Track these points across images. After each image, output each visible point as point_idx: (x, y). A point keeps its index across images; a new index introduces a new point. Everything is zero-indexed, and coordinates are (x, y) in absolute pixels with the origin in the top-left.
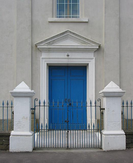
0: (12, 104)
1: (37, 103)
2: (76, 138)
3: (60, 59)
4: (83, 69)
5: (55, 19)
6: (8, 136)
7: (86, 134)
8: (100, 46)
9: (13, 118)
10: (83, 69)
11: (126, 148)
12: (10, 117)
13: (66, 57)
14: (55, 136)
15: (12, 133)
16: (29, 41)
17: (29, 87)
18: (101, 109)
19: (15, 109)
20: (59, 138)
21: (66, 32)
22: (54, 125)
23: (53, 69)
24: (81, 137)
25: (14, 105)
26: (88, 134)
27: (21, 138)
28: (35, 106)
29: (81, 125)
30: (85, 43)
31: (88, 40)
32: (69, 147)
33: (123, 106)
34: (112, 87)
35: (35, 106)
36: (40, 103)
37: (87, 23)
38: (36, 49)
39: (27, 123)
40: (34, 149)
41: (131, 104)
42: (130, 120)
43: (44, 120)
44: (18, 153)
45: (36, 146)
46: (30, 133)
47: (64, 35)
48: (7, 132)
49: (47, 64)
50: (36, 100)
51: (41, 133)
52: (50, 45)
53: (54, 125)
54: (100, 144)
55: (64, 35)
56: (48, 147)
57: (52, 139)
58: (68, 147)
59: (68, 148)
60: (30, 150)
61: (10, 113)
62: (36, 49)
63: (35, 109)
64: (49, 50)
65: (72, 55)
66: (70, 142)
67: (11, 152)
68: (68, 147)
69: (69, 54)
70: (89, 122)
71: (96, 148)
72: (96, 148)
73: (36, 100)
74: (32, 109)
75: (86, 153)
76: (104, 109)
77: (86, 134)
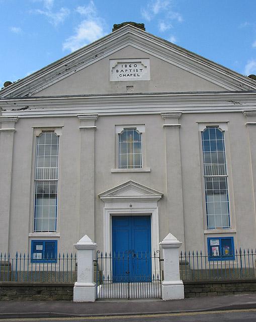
0: (75, 256)
1: (99, 256)
2: (138, 290)
3: (123, 209)
4: (147, 218)
5: (117, 170)
6: (72, 286)
7: (151, 286)
8: (163, 196)
9: (76, 270)
10: (147, 218)
11: (185, 297)
12: (73, 269)
13: (129, 207)
14: (116, 289)
15: (76, 284)
16: (92, 192)
17: (90, 240)
18: (160, 260)
19: (78, 261)
20: (120, 290)
21: (128, 182)
22: (117, 277)
23: (116, 220)
24: (146, 289)
25: (78, 257)
26: (153, 286)
27: (85, 289)
28: (97, 259)
29: (146, 277)
30: (148, 193)
31: (150, 189)
32: (131, 297)
33: (182, 257)
34: (170, 239)
35: (97, 259)
36: (102, 255)
37: (148, 174)
38: (99, 200)
39: (90, 274)
40: (96, 300)
41: (110, 255)
42: (196, 270)
43: (107, 271)
44: (82, 303)
45: (98, 297)
46: (93, 284)
47: (127, 186)
48: (71, 283)
49: (110, 214)
50: (98, 252)
51: (103, 285)
52: (113, 196)
53: (117, 277)
54: (160, 295)
55: (127, 186)
56: (114, 297)
57: (116, 290)
58: (129, 297)
59: (129, 298)
60: (93, 300)
61: (74, 265)
62: (99, 200)
63: (97, 261)
64: (112, 201)
65: (135, 205)
66: (131, 294)
67: (75, 302)
68: (129, 297)
69: (132, 204)
70: (153, 273)
71: (156, 298)
72: (156, 298)
73: (98, 252)
74: (94, 261)
75: (145, 303)
76: (163, 260)
77: (151, 286)
